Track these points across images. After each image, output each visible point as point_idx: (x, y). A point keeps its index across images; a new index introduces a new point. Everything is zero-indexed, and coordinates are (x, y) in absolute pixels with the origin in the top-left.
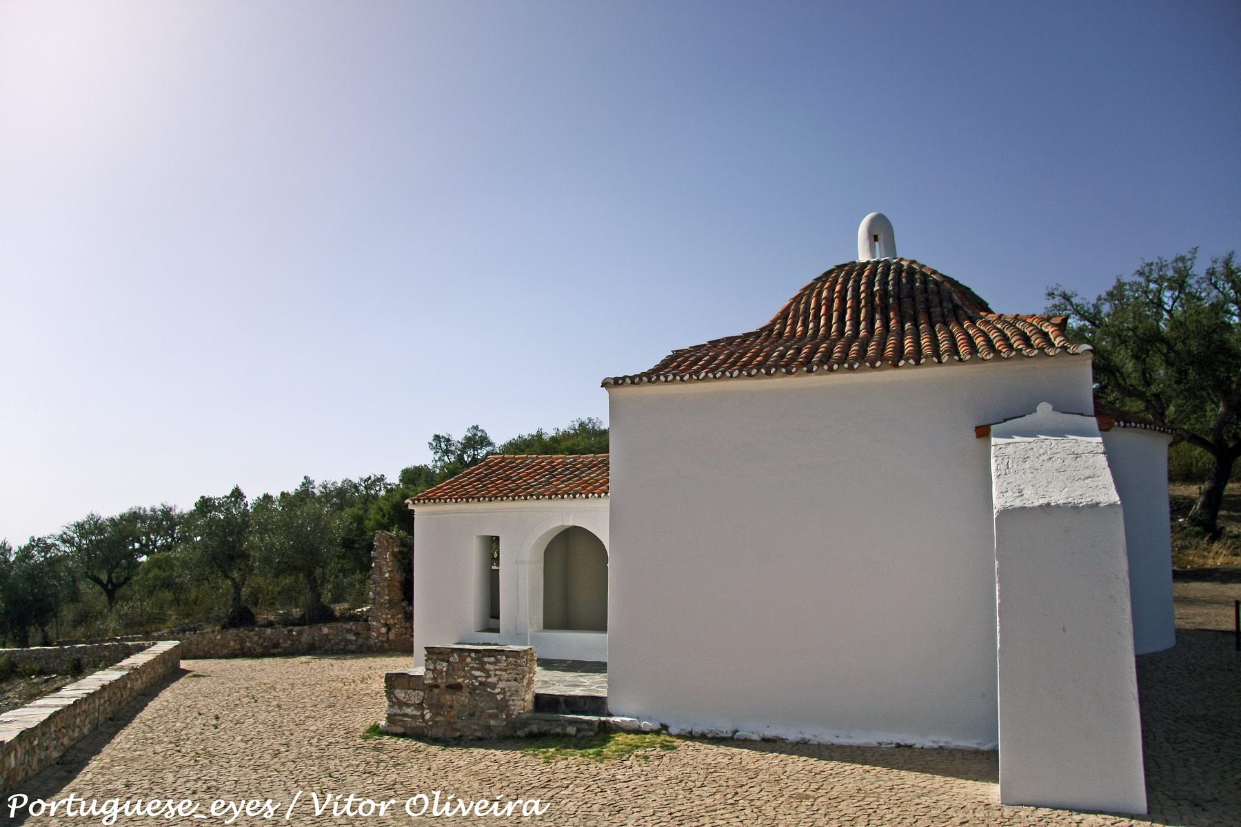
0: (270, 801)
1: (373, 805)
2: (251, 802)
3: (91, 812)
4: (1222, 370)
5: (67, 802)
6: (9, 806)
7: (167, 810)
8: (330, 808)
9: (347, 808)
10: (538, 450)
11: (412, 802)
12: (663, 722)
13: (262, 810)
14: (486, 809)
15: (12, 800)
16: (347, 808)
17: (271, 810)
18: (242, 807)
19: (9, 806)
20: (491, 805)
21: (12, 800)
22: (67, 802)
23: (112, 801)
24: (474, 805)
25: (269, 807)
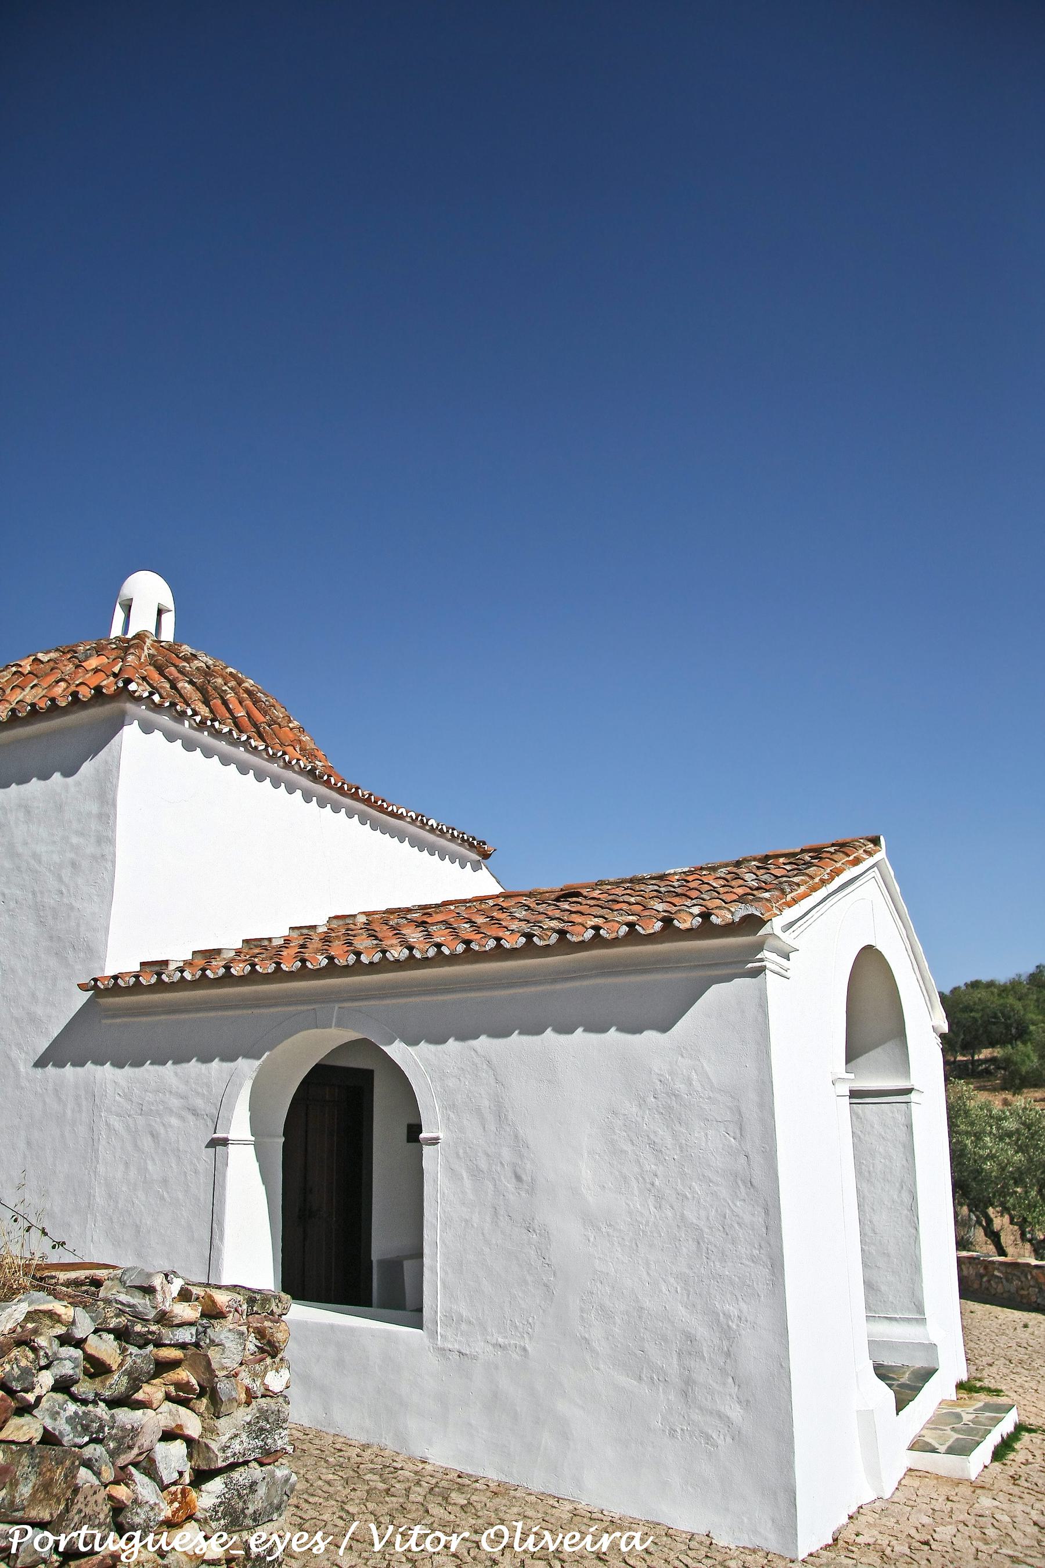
0: (320, 1534)
1: (52, 1538)
2: (569, 1535)
3: (160, 1547)
4: (1034, 1181)
5: (79, 1534)
6: (10, 1539)
7: (316, 1543)
8: (390, 1543)
9: (413, 1542)
10: (965, 1273)
11: (489, 1534)
12: (907, 1444)
13: (270, 1543)
14: (306, 1543)
15: (14, 1532)
16: (413, 1542)
17: (322, 1545)
18: (560, 1538)
19: (10, 1539)
20: (582, 1539)
21: (14, 1532)
22: (79, 1534)
23: (632, 1533)
24: (563, 1538)
25: (320, 1541)
